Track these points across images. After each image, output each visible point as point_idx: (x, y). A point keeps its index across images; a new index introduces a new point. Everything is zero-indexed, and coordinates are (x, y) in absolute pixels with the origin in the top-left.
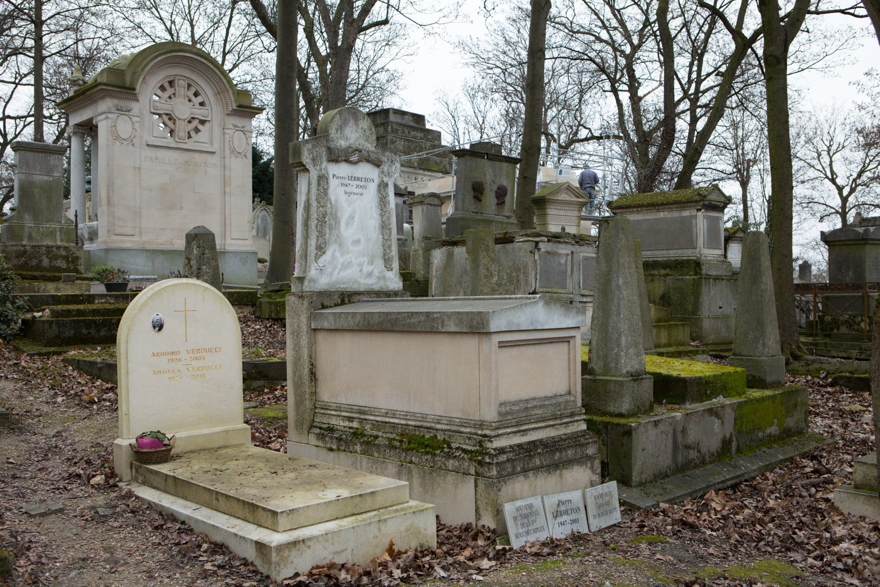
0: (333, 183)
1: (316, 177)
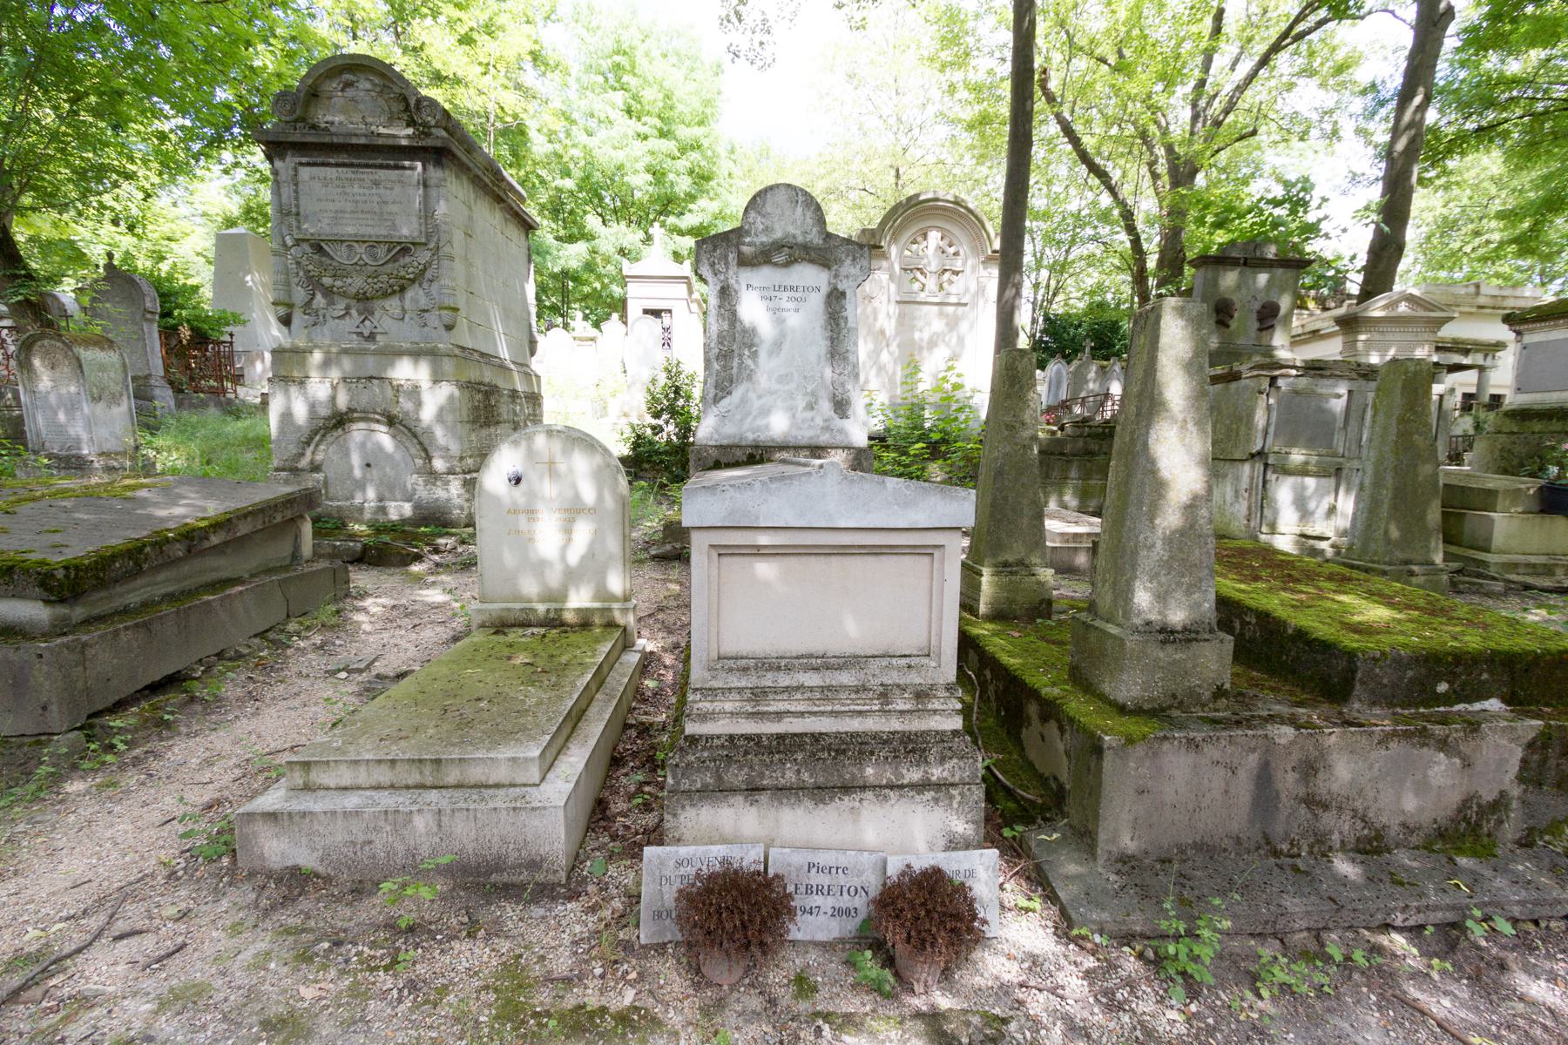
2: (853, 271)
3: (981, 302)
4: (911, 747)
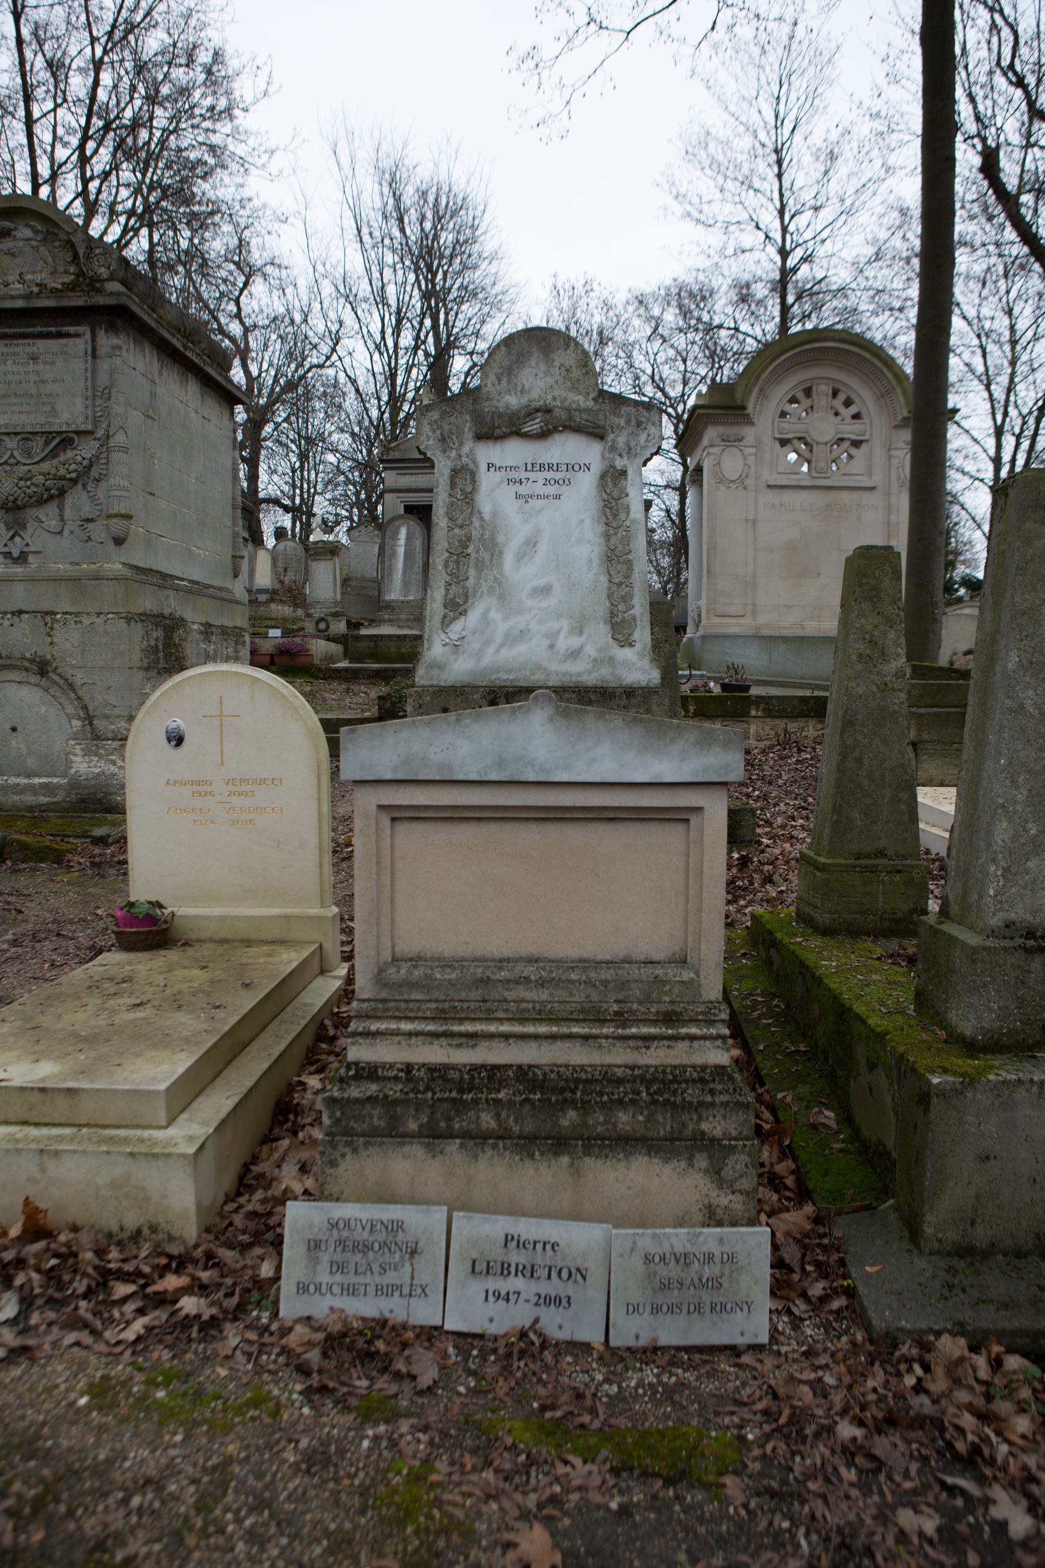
0: (487, 480)
1: (447, 472)
4: (663, 1087)
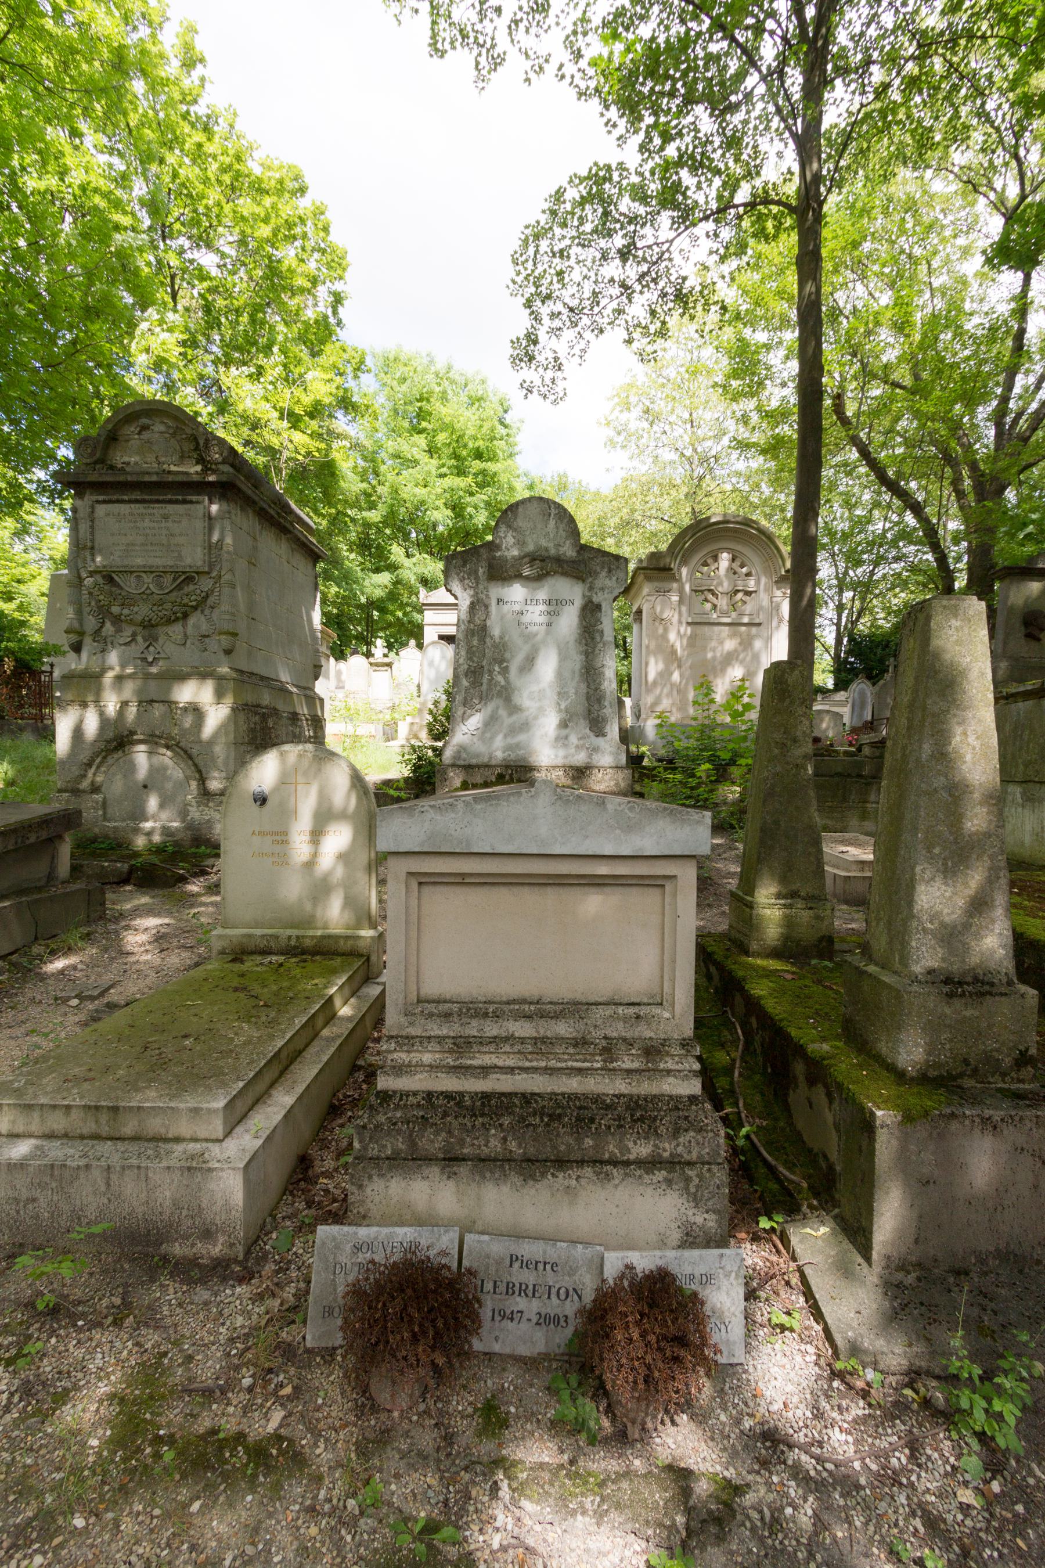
2: (608, 582)
3: (775, 623)
4: (640, 1114)
